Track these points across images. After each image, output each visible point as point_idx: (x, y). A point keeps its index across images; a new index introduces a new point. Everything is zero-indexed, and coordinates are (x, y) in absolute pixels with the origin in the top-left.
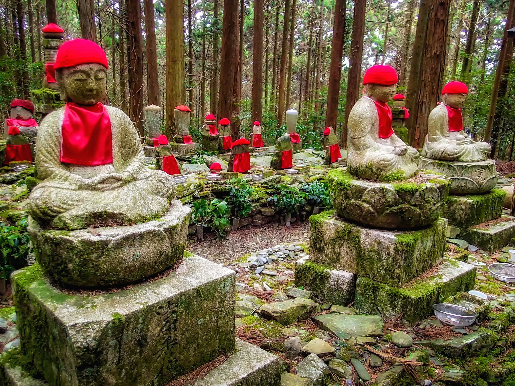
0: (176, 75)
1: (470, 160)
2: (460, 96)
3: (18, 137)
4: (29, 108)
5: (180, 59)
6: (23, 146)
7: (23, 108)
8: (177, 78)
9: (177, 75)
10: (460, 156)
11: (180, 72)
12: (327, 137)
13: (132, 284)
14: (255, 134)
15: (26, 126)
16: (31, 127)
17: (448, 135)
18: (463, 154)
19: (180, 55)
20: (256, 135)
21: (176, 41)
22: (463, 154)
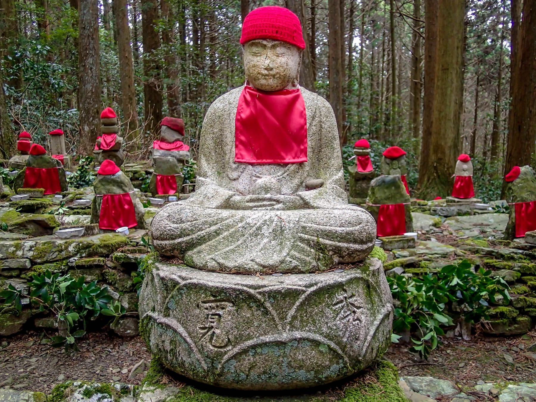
0: (446, 89)
1: (212, 264)
2: (255, 49)
3: (41, 158)
4: (175, 128)
5: (455, 66)
6: (48, 170)
7: (169, 127)
8: (449, 92)
9: (449, 89)
10: (191, 245)
11: (454, 85)
12: (510, 185)
13: (228, 389)
14: (458, 174)
15: (167, 150)
16: (172, 151)
17: (235, 175)
18: (202, 240)
19: (454, 61)
20: (459, 177)
21: (450, 41)
22: (202, 240)
